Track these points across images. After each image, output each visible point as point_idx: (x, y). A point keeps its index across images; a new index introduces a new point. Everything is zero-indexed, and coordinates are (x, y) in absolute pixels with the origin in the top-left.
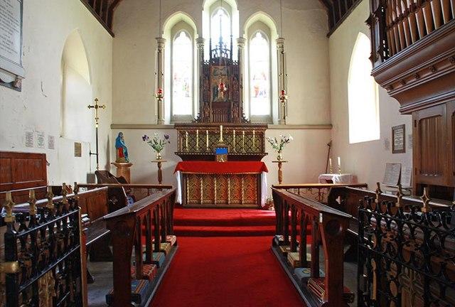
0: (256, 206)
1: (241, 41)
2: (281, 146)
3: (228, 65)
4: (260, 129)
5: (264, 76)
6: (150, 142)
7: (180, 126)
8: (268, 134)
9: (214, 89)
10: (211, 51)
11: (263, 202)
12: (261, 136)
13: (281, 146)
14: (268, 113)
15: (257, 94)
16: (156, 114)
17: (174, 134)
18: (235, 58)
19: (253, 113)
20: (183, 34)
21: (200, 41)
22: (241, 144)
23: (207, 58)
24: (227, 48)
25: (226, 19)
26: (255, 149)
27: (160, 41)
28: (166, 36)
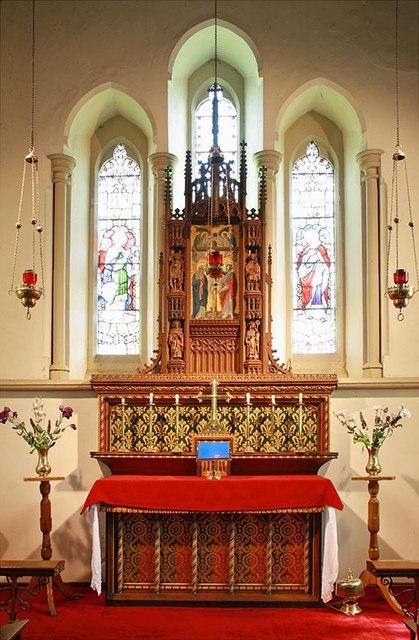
0: (305, 598)
1: (266, 160)
2: (378, 436)
3: (235, 220)
4: (316, 394)
5: (325, 254)
6: (21, 426)
7: (112, 390)
8: (336, 405)
9: (196, 286)
10: (189, 185)
11: (326, 595)
12: (318, 407)
13: (378, 436)
14: (330, 349)
15: (305, 304)
16: (381, 187)
17: (90, 409)
18: (252, 202)
19: (299, 348)
20: (120, 153)
21: (164, 163)
22: (264, 434)
23: (179, 202)
24: (232, 176)
25: (226, 108)
26: (301, 448)
27: (60, 166)
28: (76, 148)
